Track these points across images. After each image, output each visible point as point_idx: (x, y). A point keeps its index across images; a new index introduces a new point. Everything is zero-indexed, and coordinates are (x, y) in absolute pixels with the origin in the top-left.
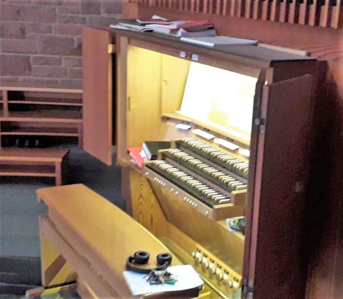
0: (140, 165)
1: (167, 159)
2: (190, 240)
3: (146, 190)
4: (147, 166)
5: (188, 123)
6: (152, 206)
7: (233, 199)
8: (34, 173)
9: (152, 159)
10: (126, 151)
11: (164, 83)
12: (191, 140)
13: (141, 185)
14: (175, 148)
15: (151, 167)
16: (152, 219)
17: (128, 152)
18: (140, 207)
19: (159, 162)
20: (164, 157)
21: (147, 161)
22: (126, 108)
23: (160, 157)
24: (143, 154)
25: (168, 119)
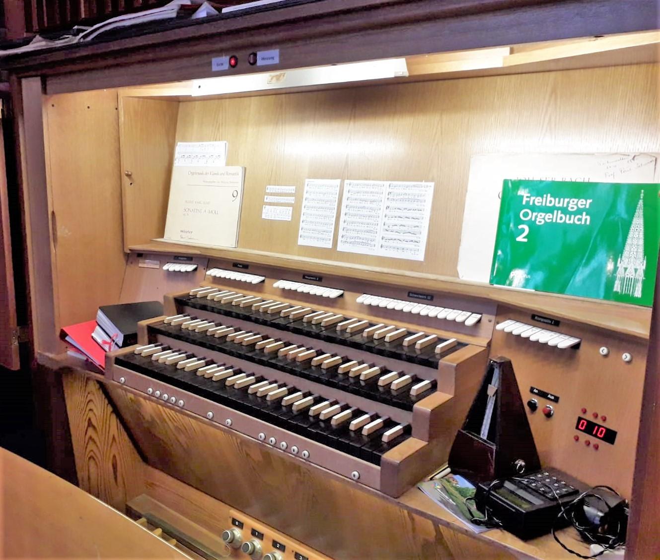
0: (98, 361)
1: (161, 338)
2: (209, 502)
3: (99, 408)
4: (118, 361)
5: (189, 258)
6: (114, 438)
7: (422, 428)
8: (119, 27)
9: (126, 344)
10: (58, 333)
11: (126, 180)
12: (201, 289)
13: (89, 401)
14: (175, 311)
15: (123, 362)
16: (115, 467)
17: (63, 335)
18: (91, 446)
19: (143, 349)
20: (154, 334)
21: (116, 352)
22: (48, 236)
23: (144, 336)
24: (98, 335)
25: (140, 255)
